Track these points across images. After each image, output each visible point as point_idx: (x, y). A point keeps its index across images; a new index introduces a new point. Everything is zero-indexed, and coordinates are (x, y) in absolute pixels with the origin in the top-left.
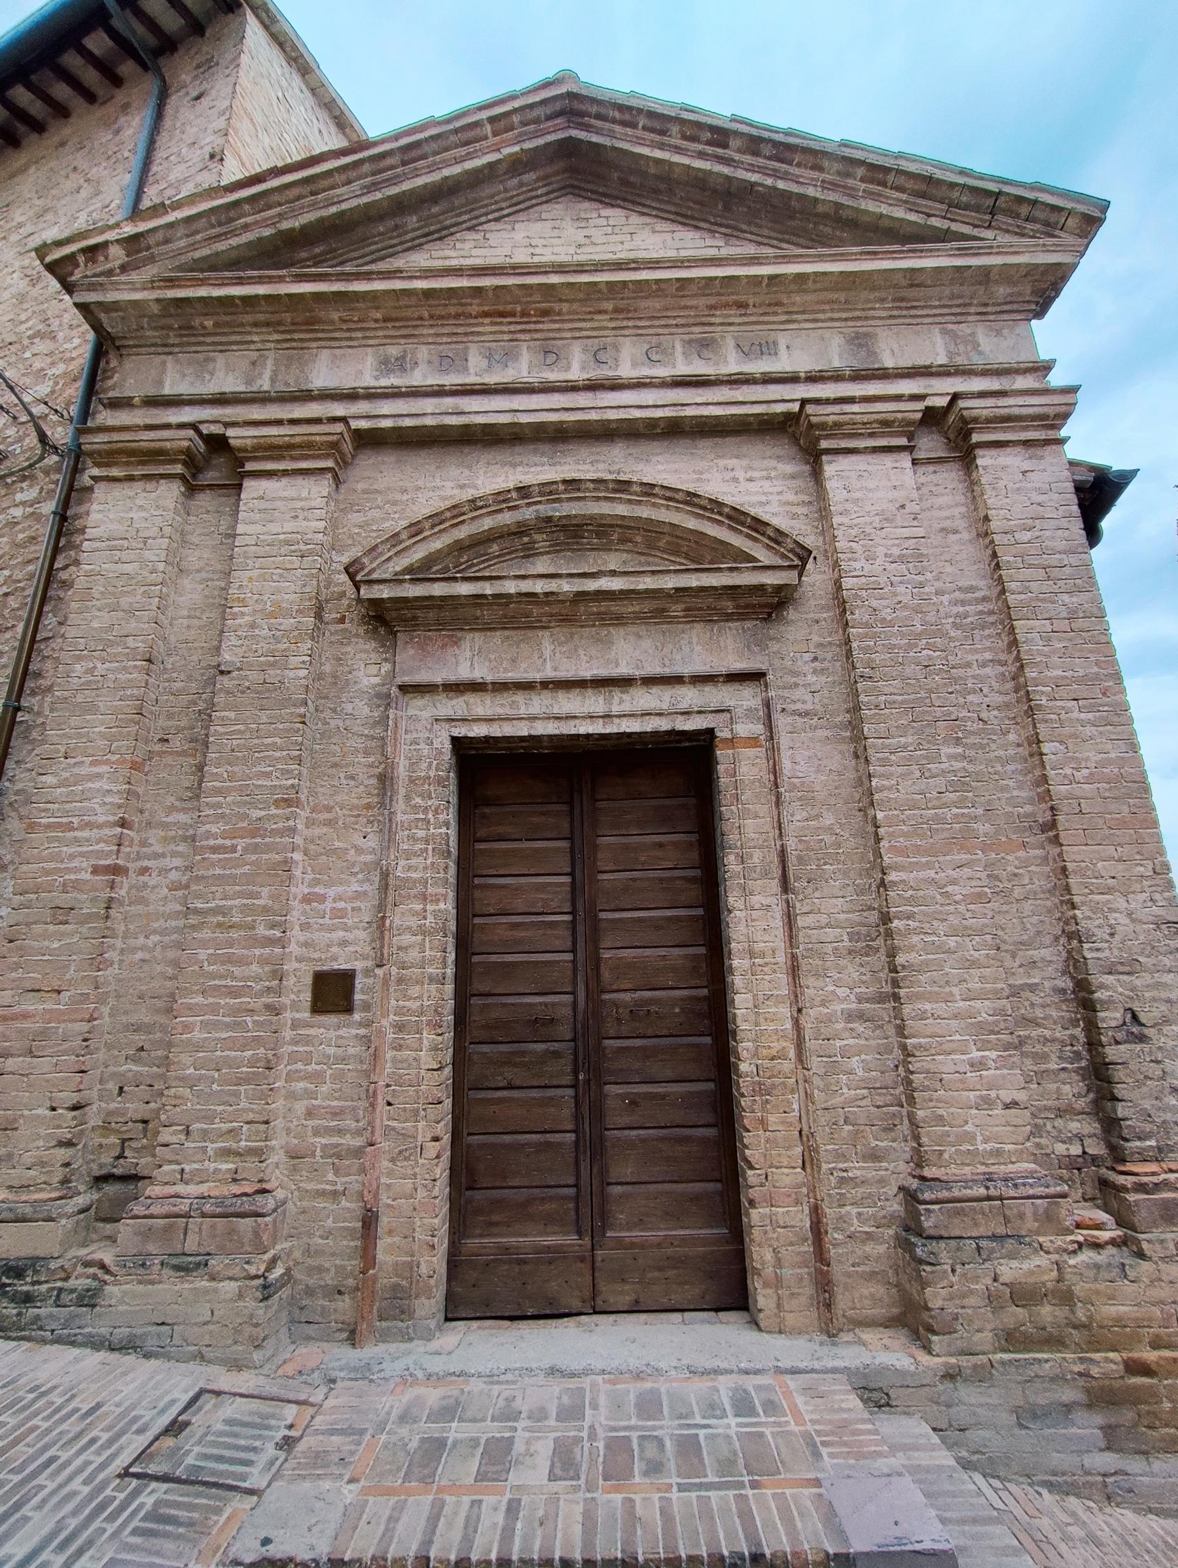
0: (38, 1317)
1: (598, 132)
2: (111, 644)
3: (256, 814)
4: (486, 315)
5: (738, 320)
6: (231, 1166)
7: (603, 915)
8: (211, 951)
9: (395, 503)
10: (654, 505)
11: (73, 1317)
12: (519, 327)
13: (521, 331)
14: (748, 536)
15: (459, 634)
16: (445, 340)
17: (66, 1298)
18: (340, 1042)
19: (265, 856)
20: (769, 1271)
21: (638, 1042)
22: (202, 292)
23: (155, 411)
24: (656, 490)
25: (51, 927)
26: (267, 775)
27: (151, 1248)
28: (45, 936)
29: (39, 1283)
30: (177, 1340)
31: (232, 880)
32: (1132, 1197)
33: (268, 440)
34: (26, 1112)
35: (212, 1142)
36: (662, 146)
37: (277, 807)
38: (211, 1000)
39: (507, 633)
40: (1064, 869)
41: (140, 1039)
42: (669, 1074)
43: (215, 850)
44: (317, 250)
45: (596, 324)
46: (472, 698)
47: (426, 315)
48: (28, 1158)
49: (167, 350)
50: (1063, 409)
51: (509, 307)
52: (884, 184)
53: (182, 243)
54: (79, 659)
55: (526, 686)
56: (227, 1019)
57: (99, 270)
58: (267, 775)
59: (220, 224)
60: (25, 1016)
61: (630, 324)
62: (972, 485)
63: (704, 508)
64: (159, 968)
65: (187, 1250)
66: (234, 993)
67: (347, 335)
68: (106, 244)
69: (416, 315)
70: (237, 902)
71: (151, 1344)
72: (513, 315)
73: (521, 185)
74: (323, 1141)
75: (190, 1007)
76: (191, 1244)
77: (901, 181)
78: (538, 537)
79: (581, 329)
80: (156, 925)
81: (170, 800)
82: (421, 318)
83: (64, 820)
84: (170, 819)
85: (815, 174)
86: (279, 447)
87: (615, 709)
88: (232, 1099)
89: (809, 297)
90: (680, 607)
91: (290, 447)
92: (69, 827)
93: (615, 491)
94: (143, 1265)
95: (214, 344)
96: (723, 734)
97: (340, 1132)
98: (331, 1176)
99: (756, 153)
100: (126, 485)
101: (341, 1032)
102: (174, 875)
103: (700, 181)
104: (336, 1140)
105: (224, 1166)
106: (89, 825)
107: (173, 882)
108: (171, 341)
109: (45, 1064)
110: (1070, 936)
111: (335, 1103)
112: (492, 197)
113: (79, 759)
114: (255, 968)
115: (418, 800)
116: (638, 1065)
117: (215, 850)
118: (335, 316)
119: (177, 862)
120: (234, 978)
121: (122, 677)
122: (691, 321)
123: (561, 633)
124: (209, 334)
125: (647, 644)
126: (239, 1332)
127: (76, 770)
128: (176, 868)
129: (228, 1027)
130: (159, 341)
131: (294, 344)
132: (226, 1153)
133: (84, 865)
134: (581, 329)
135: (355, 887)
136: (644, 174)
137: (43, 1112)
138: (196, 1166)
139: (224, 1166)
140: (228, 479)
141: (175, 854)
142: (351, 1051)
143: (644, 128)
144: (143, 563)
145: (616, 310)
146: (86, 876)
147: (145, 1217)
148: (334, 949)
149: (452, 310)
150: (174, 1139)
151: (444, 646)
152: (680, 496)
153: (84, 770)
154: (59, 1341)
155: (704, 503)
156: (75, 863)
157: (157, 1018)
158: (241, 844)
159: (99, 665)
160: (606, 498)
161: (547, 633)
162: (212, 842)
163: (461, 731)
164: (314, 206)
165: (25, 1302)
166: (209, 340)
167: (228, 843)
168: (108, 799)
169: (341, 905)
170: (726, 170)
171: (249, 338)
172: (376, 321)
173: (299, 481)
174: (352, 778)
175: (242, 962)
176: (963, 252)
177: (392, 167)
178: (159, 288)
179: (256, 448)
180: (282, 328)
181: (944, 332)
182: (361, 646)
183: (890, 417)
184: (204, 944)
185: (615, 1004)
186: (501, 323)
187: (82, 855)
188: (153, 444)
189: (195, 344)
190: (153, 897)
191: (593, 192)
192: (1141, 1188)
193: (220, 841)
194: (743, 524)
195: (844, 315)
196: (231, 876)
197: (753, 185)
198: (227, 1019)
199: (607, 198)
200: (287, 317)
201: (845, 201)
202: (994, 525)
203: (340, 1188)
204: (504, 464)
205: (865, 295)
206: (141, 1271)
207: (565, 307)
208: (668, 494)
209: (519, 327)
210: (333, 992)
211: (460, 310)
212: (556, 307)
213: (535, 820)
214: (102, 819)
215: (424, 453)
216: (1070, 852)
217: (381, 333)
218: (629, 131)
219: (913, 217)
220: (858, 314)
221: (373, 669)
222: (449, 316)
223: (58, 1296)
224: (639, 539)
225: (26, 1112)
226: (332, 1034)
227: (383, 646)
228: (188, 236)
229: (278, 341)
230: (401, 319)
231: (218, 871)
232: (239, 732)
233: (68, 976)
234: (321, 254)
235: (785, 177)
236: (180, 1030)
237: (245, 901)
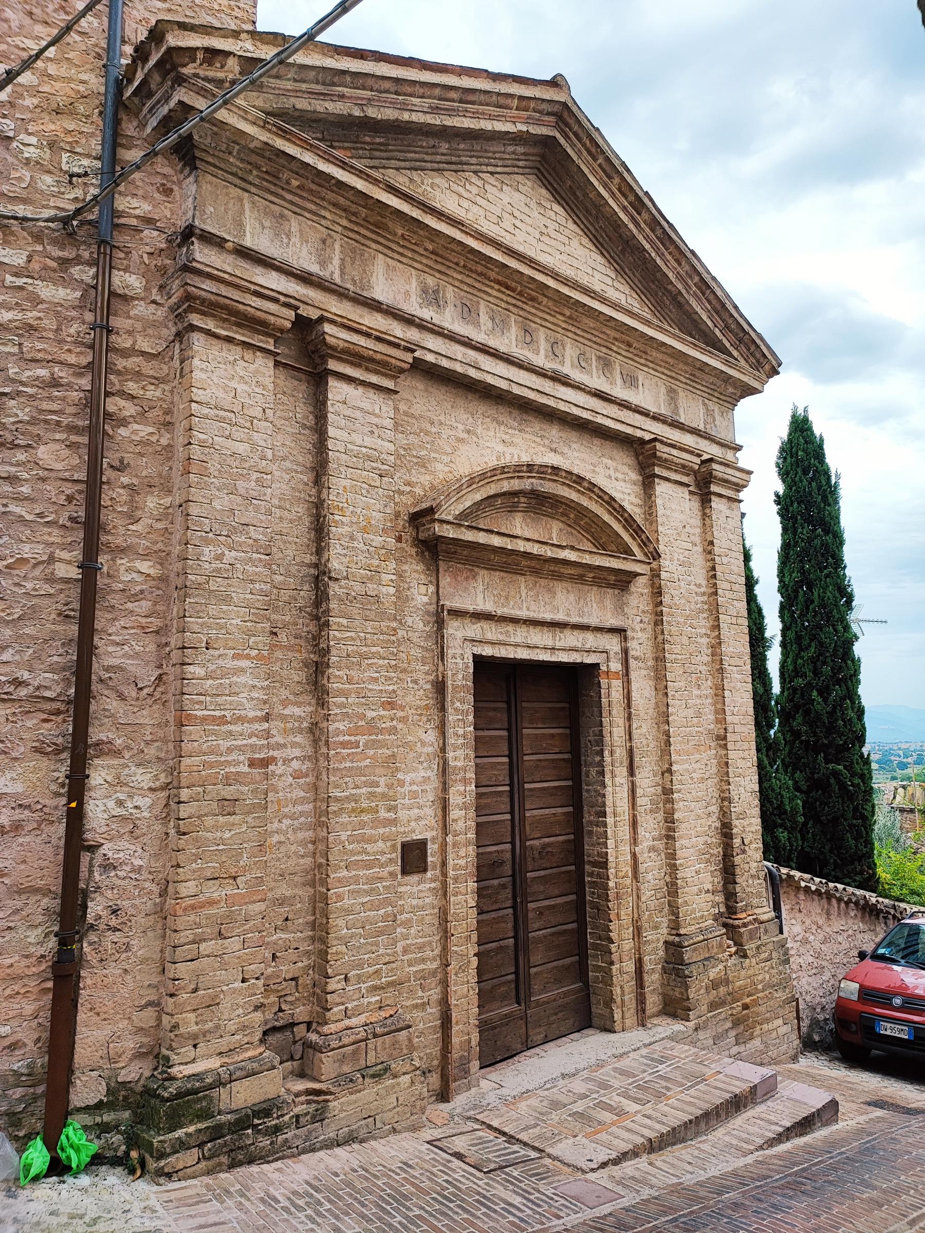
0: (286, 1140)
1: (573, 146)
2: (235, 530)
3: (370, 714)
4: (499, 282)
5: (624, 353)
6: (378, 998)
7: (527, 786)
8: (349, 833)
9: (427, 433)
10: (590, 498)
11: (310, 1132)
12: (514, 302)
13: (515, 305)
14: (631, 535)
15: (476, 569)
16: (465, 288)
17: (303, 1120)
18: (421, 895)
19: (380, 751)
20: (618, 1000)
21: (542, 873)
22: (308, 158)
23: (241, 263)
24: (596, 489)
25: (221, 818)
26: (376, 680)
27: (346, 1069)
28: (217, 827)
29: (282, 1116)
30: (379, 1125)
31: (361, 772)
32: (742, 930)
33: (357, 349)
34: (225, 988)
35: (364, 982)
36: (605, 186)
37: (384, 709)
38: (353, 873)
39: (502, 574)
40: (727, 763)
41: (283, 910)
42: (557, 892)
43: (344, 745)
44: (378, 140)
45: (555, 321)
46: (485, 624)
47: (462, 264)
48: (232, 1026)
49: (243, 185)
50: (741, 482)
51: (514, 284)
52: (704, 294)
53: (289, 85)
54: (207, 542)
55: (515, 621)
56: (365, 887)
57: (211, 74)
58: (376, 680)
59: (324, 84)
60: (212, 903)
61: (573, 329)
62: (705, 516)
63: (615, 509)
64: (293, 848)
65: (369, 1064)
66: (368, 865)
67: (401, 250)
68: (227, 54)
69: (456, 260)
70: (364, 790)
71: (362, 1133)
72: (513, 290)
73: (513, 153)
74: (414, 969)
75: (340, 880)
76: (371, 1059)
77: (711, 297)
78: (522, 500)
79: (546, 320)
80: (286, 810)
81: (284, 693)
82: (457, 264)
83: (217, 713)
84: (286, 712)
85: (676, 265)
86: (362, 357)
87: (558, 644)
88: (374, 948)
89: (660, 356)
90: (592, 575)
91: (371, 360)
92: (222, 721)
93: (575, 482)
94: (351, 1081)
95: (292, 203)
96: (603, 668)
97: (423, 960)
98: (420, 994)
99: (653, 230)
100: (226, 346)
101: (420, 887)
102: (295, 764)
103: (617, 224)
104: (422, 967)
105: (373, 999)
106: (241, 719)
107: (295, 771)
108: (251, 178)
109: (234, 944)
110: (723, 799)
111: (420, 940)
112: (494, 153)
113: (222, 651)
114: (380, 844)
115: (458, 704)
116: (542, 889)
117: (344, 745)
118: (400, 232)
119: (297, 752)
120: (368, 854)
121: (250, 569)
122: (603, 342)
123: (531, 579)
124: (290, 192)
125: (572, 597)
126: (414, 1106)
127: (220, 662)
128: (296, 758)
129: (368, 893)
130: (240, 173)
131: (357, 237)
132: (375, 989)
133: (242, 758)
134: (546, 320)
135: (423, 773)
136: (586, 195)
137: (238, 985)
138: (355, 1003)
139: (373, 999)
140: (297, 361)
141: (294, 745)
142: (427, 900)
143: (600, 165)
144: (254, 446)
145: (570, 318)
146: (246, 769)
147: (340, 1047)
148: (413, 824)
149: (480, 269)
150: (340, 986)
151: (467, 578)
152: (606, 498)
153: (230, 664)
154: (304, 1152)
155: (616, 506)
156: (233, 757)
157: (296, 891)
158: (362, 739)
159: (227, 552)
160: (568, 485)
161: (522, 579)
162: (341, 738)
163: (479, 650)
164: (393, 105)
165: (275, 1133)
166: (289, 197)
167: (353, 738)
168: (255, 695)
169: (414, 788)
170: (635, 231)
171: (323, 213)
172: (426, 250)
173: (371, 393)
174: (416, 683)
175: (371, 840)
176: (726, 363)
177: (453, 101)
178: (269, 131)
179: (344, 351)
180: (354, 219)
181: (704, 404)
182: (414, 567)
183: (687, 463)
184: (344, 827)
185: (532, 847)
186: (504, 293)
187: (239, 748)
188: (259, 314)
189: (272, 193)
190: (281, 784)
191: (550, 183)
192: (745, 925)
193: (347, 738)
194: (631, 527)
195: (666, 371)
196: (358, 768)
197: (644, 250)
198: (365, 887)
199: (558, 196)
200: (364, 212)
201: (684, 291)
202: (717, 550)
203: (426, 1000)
204: (495, 420)
205: (681, 366)
206: (352, 1085)
207: (545, 301)
208: (601, 494)
209: (514, 302)
210: (413, 857)
211: (485, 271)
212: (541, 298)
213: (491, 714)
214: (251, 714)
215: (444, 389)
216: (731, 754)
217: (424, 261)
218: (591, 161)
219: (710, 323)
220: (674, 375)
221: (423, 589)
222: (476, 272)
223: (297, 1122)
224: (572, 516)
225: (225, 988)
226: (415, 889)
227: (428, 569)
228: (295, 80)
229: (345, 228)
230: (441, 257)
231: (348, 764)
232: (352, 639)
233: (242, 863)
234: (380, 144)
235: (661, 256)
236: (334, 900)
237: (370, 790)
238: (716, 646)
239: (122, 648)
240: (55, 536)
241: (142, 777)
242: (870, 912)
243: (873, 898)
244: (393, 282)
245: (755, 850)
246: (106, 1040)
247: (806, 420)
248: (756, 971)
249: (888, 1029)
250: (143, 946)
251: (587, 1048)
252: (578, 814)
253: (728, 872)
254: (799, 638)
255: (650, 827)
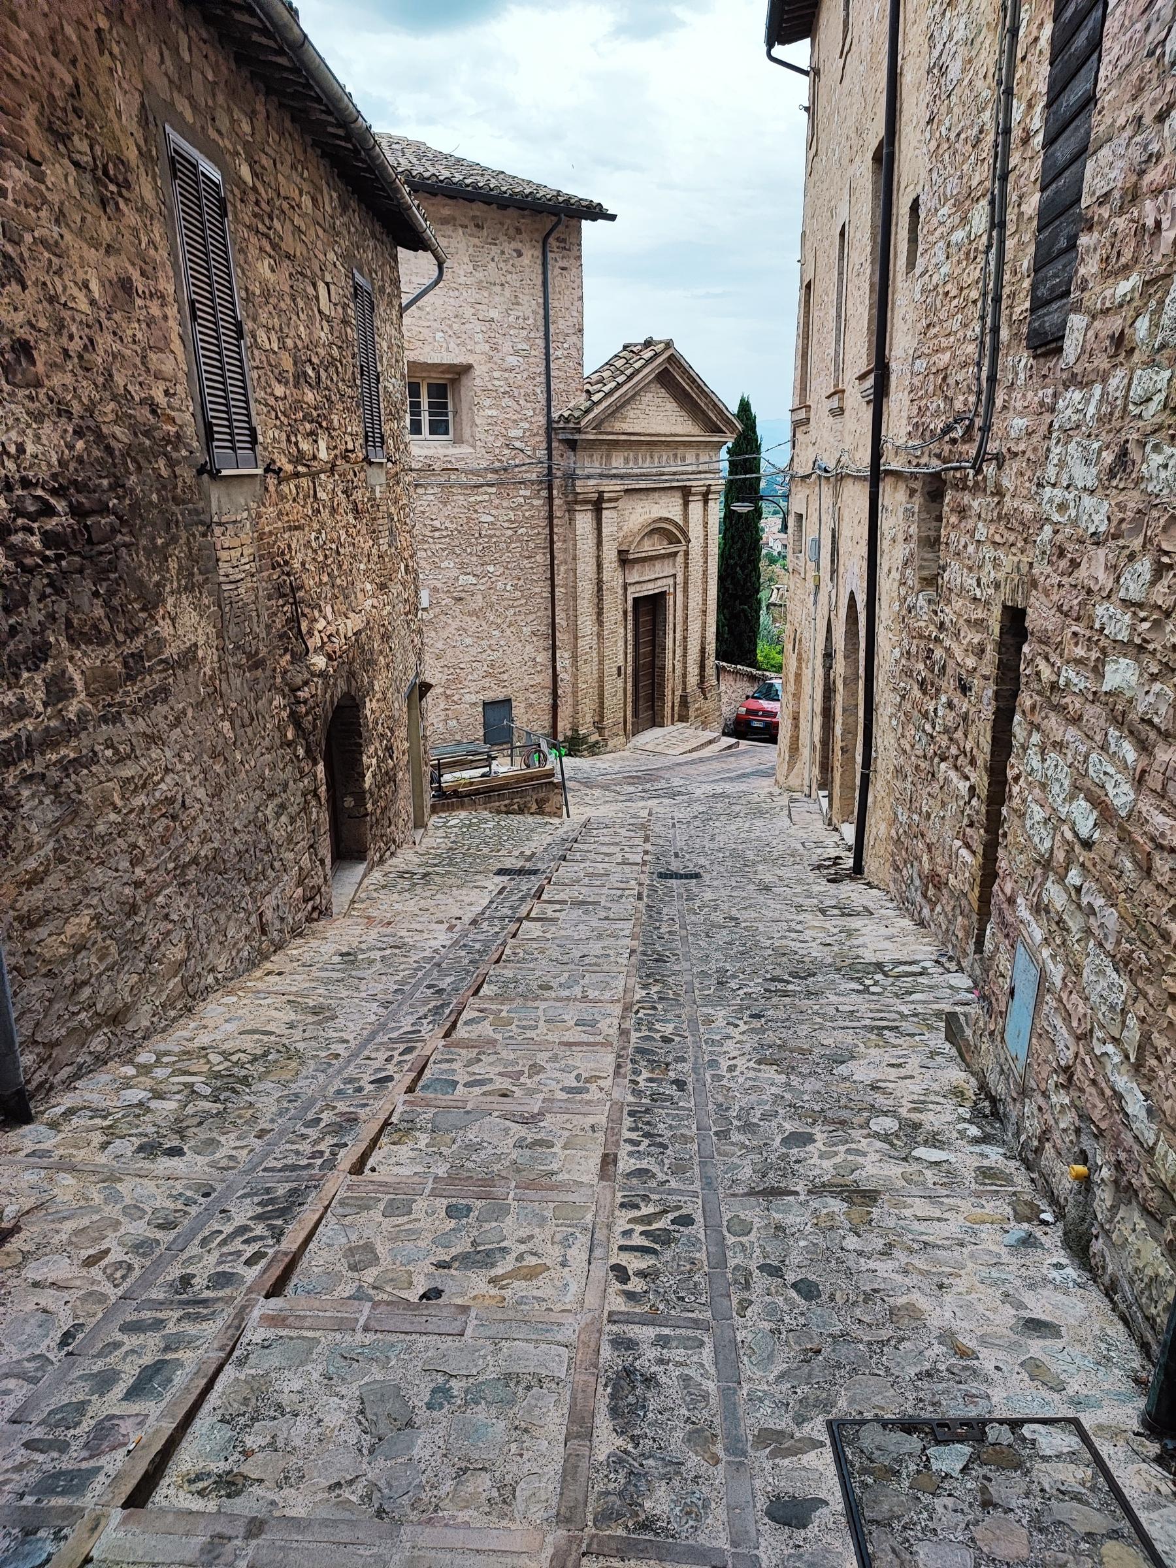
238: (705, 571)
239: (560, 619)
240: (541, 584)
241: (566, 655)
242: (752, 678)
243: (754, 672)
244: (618, 462)
245: (712, 658)
246: (563, 725)
247: (748, 404)
248: (710, 704)
249: (756, 724)
250: (570, 701)
251: (657, 732)
252: (654, 650)
253: (702, 667)
254: (733, 537)
255: (679, 651)
